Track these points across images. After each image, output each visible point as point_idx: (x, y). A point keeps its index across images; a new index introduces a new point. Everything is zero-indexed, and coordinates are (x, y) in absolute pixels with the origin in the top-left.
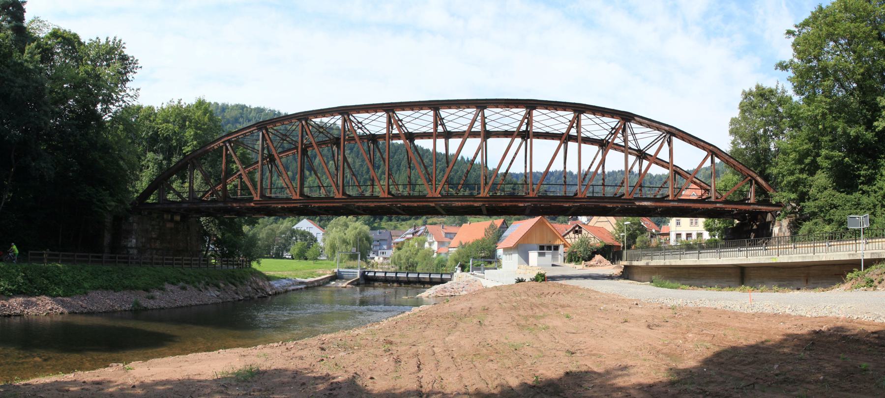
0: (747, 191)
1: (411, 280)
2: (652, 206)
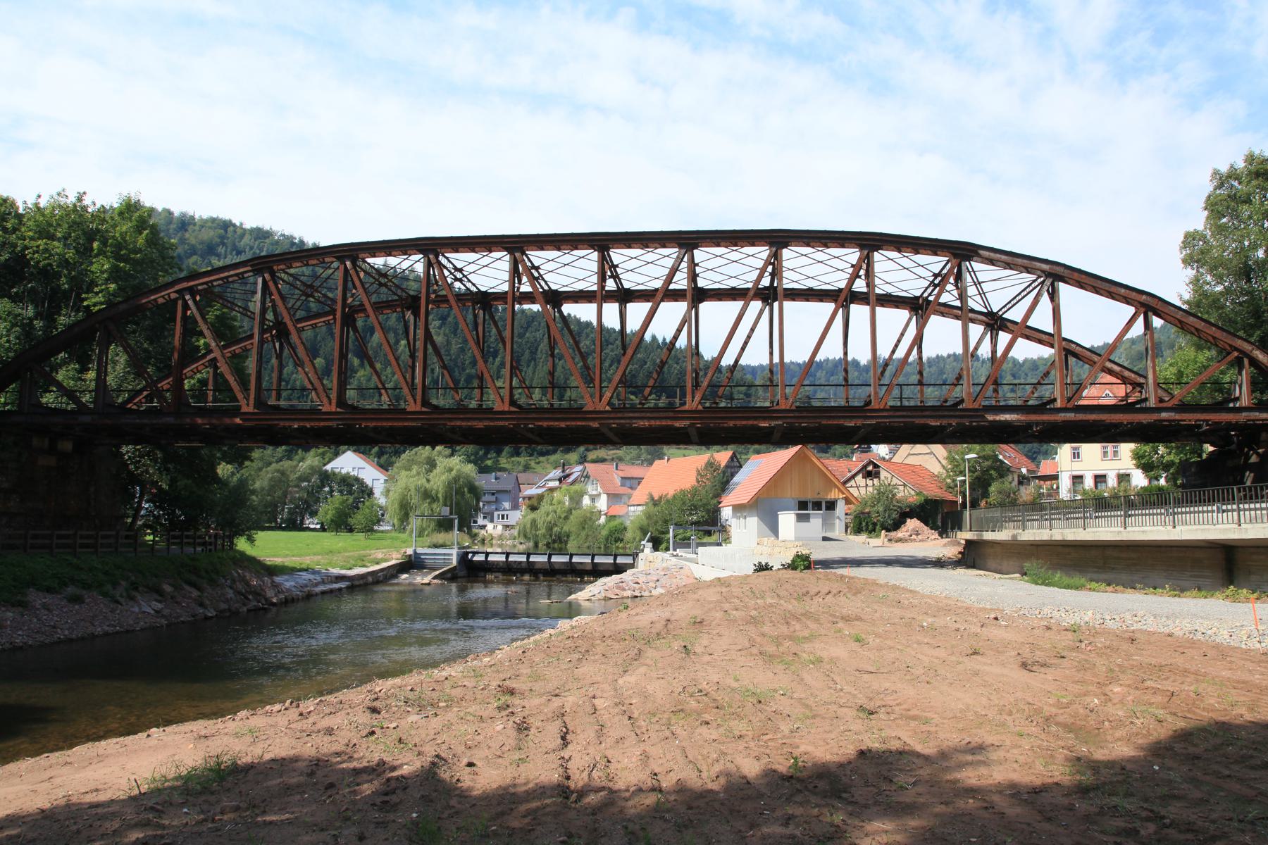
0: (1231, 383)
1: (557, 567)
2: (1019, 421)
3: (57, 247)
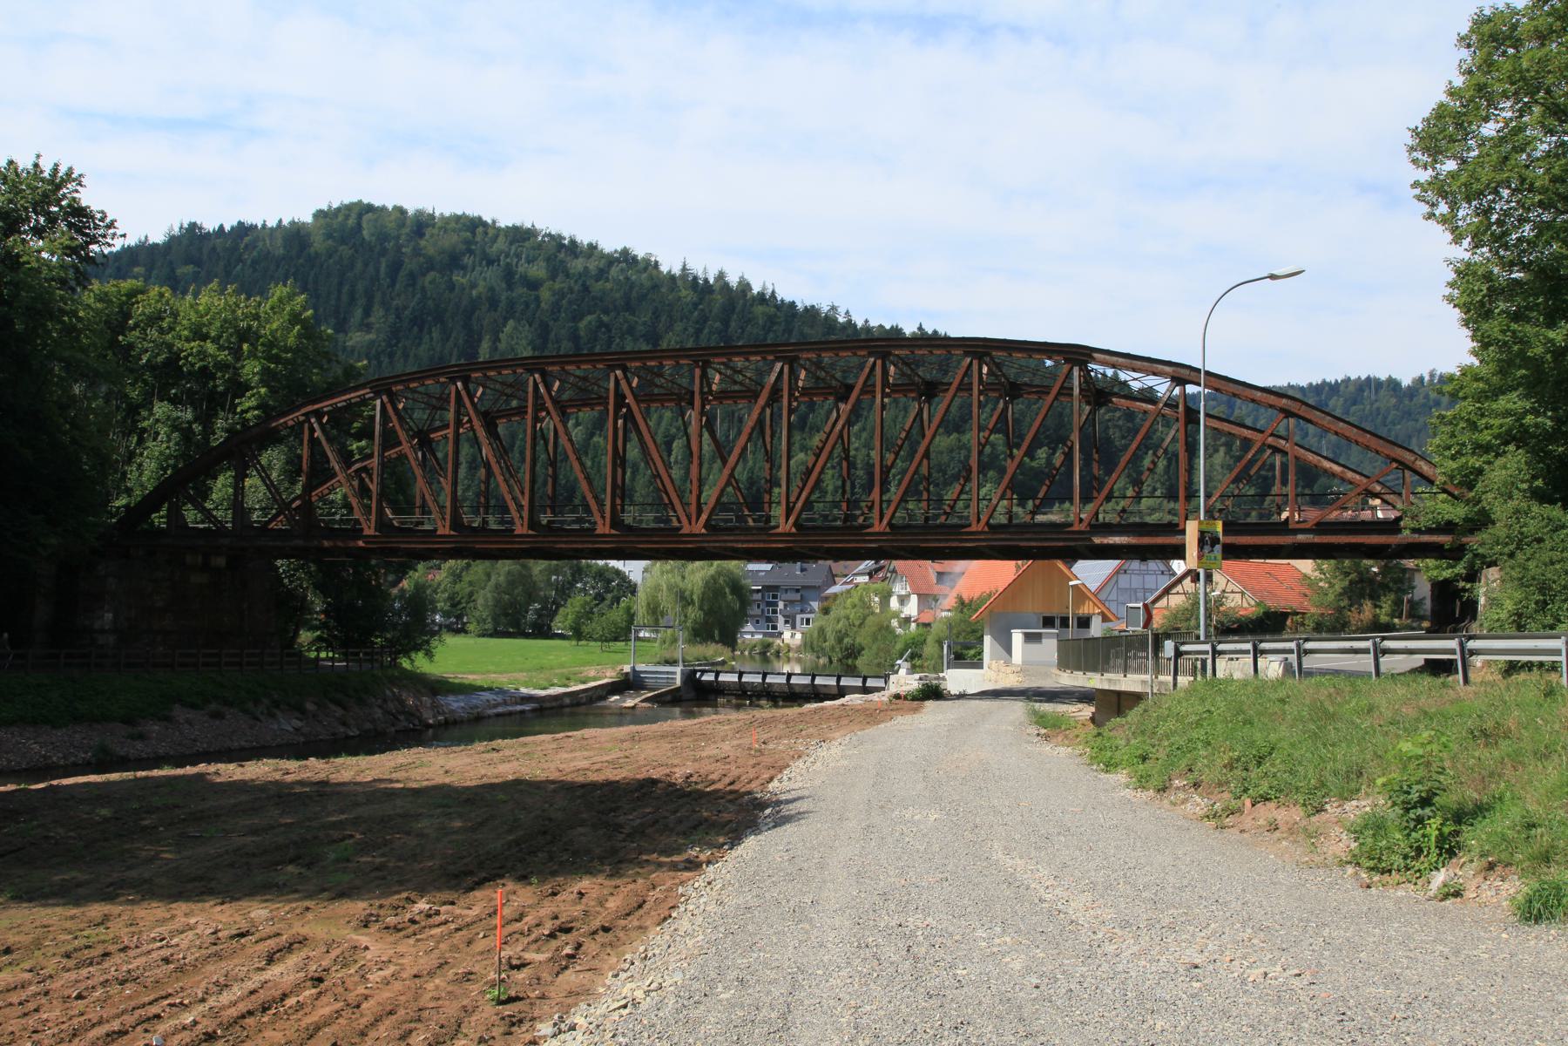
1: (797, 690)
3: (210, 347)
